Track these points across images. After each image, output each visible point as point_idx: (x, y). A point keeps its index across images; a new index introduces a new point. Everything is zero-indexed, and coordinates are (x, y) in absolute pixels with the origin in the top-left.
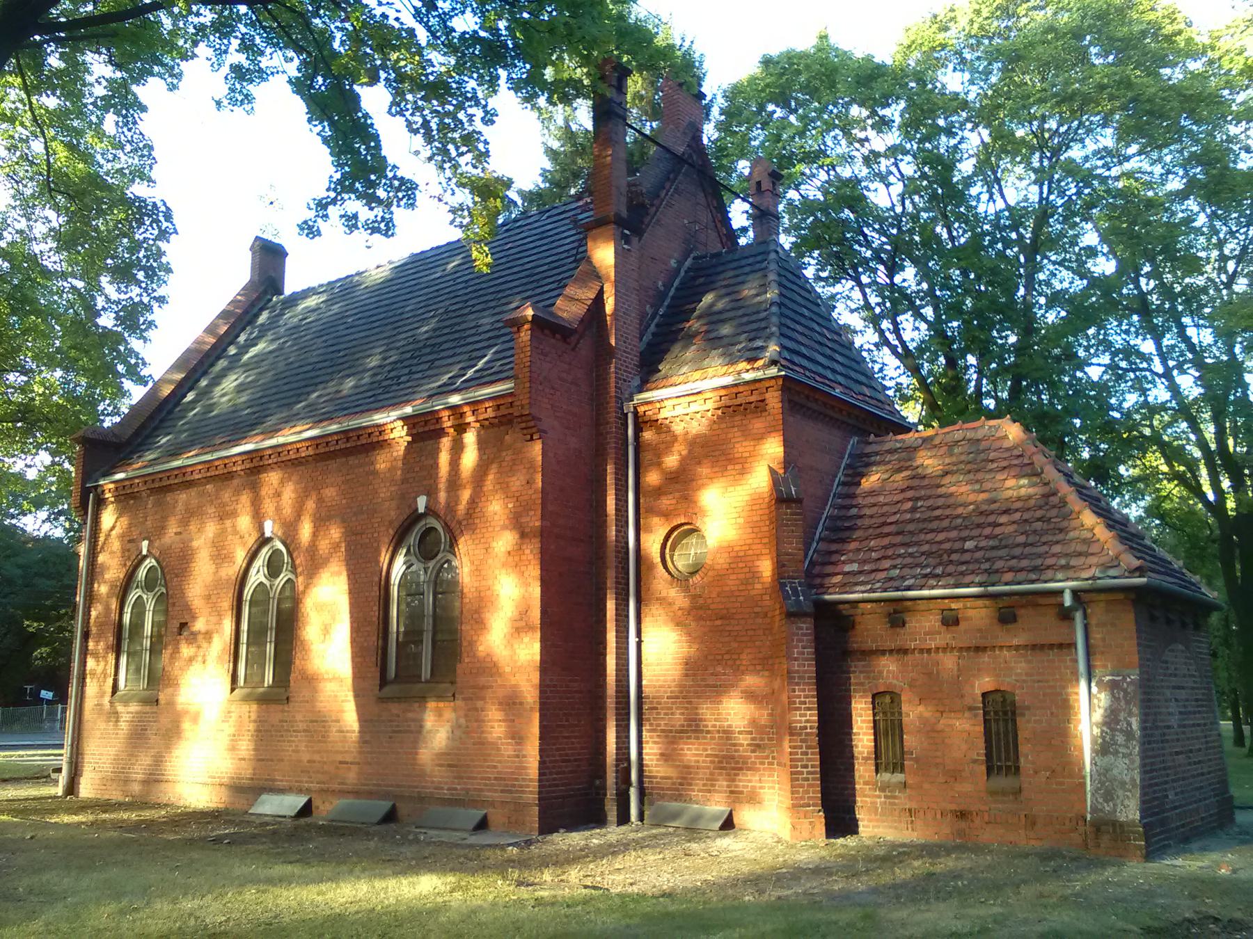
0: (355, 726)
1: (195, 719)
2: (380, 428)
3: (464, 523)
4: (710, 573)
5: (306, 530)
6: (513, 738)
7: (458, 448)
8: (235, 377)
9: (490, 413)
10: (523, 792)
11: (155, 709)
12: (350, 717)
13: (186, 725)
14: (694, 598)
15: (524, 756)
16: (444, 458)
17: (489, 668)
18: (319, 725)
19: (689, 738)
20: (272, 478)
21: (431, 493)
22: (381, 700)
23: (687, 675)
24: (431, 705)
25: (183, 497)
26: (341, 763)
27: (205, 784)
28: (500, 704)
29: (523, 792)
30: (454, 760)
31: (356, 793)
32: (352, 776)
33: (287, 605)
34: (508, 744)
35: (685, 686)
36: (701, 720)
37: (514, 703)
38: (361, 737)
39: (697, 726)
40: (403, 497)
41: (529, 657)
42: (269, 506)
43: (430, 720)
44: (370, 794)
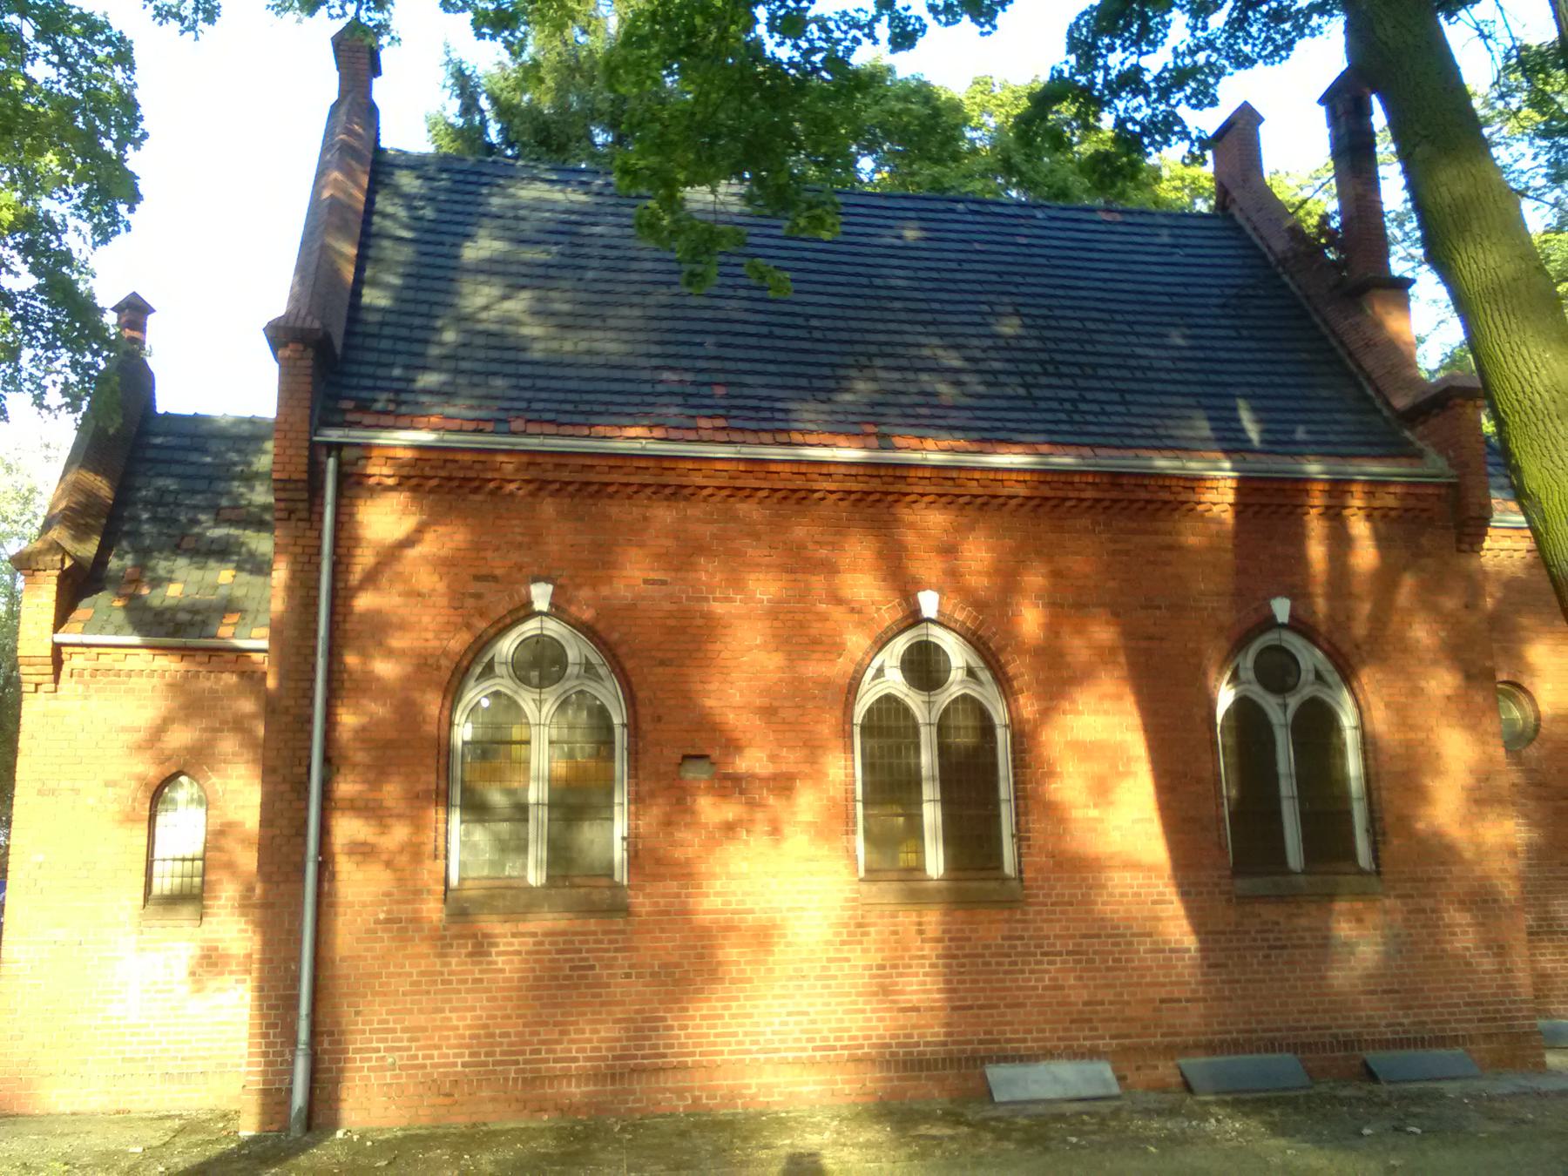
0: (1190, 942)
1: (763, 937)
2: (1194, 482)
3: (1366, 647)
4: (1549, 745)
5: (1030, 620)
6: (1489, 948)
7: (1340, 541)
8: (1481, 313)
9: (1391, 501)
10: (1516, 1018)
11: (619, 923)
12: (1177, 929)
13: (731, 953)
14: (1529, 771)
15: (1510, 971)
16: (1317, 551)
17: (1438, 852)
18: (1107, 944)
19: (1542, 940)
20: (929, 522)
21: (1299, 595)
22: (1244, 899)
23: (1530, 865)
24: (1341, 905)
25: (664, 514)
26: (1162, 1001)
27: (812, 1062)
28: (1462, 902)
29: (1516, 1018)
30: (1394, 983)
31: (1211, 1048)
32: (1192, 1019)
33: (964, 739)
34: (1481, 956)
35: (1528, 879)
36: (1553, 919)
37: (1486, 901)
38: (1204, 958)
39: (1550, 926)
40: (1239, 594)
41: (1499, 840)
42: (927, 566)
43: (1344, 929)
44: (1236, 1047)
